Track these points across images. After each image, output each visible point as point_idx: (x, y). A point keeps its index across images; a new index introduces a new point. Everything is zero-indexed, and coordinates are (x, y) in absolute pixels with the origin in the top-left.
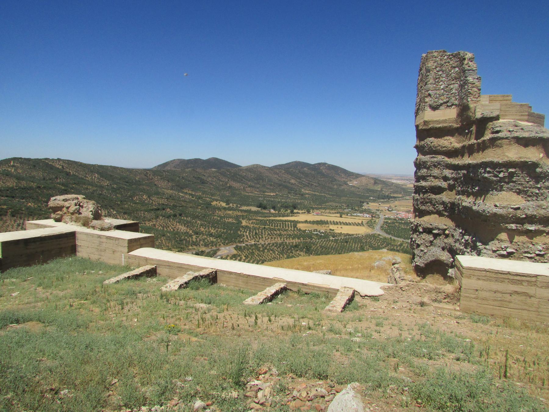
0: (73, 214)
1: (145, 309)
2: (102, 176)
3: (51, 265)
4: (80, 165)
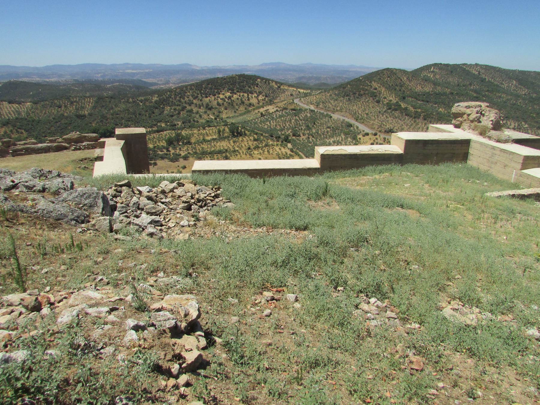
0: (472, 121)
1: (518, 230)
2: (521, 84)
3: (442, 167)
4: (498, 71)
